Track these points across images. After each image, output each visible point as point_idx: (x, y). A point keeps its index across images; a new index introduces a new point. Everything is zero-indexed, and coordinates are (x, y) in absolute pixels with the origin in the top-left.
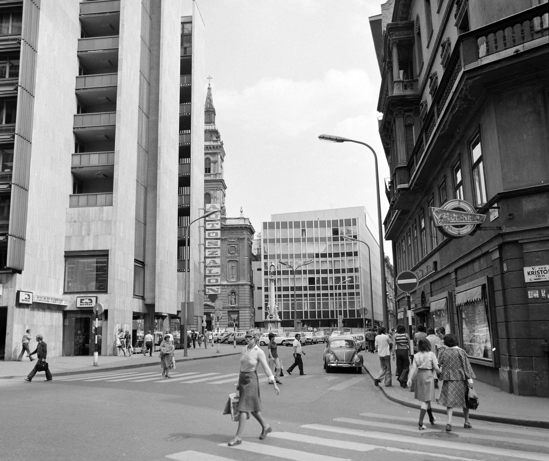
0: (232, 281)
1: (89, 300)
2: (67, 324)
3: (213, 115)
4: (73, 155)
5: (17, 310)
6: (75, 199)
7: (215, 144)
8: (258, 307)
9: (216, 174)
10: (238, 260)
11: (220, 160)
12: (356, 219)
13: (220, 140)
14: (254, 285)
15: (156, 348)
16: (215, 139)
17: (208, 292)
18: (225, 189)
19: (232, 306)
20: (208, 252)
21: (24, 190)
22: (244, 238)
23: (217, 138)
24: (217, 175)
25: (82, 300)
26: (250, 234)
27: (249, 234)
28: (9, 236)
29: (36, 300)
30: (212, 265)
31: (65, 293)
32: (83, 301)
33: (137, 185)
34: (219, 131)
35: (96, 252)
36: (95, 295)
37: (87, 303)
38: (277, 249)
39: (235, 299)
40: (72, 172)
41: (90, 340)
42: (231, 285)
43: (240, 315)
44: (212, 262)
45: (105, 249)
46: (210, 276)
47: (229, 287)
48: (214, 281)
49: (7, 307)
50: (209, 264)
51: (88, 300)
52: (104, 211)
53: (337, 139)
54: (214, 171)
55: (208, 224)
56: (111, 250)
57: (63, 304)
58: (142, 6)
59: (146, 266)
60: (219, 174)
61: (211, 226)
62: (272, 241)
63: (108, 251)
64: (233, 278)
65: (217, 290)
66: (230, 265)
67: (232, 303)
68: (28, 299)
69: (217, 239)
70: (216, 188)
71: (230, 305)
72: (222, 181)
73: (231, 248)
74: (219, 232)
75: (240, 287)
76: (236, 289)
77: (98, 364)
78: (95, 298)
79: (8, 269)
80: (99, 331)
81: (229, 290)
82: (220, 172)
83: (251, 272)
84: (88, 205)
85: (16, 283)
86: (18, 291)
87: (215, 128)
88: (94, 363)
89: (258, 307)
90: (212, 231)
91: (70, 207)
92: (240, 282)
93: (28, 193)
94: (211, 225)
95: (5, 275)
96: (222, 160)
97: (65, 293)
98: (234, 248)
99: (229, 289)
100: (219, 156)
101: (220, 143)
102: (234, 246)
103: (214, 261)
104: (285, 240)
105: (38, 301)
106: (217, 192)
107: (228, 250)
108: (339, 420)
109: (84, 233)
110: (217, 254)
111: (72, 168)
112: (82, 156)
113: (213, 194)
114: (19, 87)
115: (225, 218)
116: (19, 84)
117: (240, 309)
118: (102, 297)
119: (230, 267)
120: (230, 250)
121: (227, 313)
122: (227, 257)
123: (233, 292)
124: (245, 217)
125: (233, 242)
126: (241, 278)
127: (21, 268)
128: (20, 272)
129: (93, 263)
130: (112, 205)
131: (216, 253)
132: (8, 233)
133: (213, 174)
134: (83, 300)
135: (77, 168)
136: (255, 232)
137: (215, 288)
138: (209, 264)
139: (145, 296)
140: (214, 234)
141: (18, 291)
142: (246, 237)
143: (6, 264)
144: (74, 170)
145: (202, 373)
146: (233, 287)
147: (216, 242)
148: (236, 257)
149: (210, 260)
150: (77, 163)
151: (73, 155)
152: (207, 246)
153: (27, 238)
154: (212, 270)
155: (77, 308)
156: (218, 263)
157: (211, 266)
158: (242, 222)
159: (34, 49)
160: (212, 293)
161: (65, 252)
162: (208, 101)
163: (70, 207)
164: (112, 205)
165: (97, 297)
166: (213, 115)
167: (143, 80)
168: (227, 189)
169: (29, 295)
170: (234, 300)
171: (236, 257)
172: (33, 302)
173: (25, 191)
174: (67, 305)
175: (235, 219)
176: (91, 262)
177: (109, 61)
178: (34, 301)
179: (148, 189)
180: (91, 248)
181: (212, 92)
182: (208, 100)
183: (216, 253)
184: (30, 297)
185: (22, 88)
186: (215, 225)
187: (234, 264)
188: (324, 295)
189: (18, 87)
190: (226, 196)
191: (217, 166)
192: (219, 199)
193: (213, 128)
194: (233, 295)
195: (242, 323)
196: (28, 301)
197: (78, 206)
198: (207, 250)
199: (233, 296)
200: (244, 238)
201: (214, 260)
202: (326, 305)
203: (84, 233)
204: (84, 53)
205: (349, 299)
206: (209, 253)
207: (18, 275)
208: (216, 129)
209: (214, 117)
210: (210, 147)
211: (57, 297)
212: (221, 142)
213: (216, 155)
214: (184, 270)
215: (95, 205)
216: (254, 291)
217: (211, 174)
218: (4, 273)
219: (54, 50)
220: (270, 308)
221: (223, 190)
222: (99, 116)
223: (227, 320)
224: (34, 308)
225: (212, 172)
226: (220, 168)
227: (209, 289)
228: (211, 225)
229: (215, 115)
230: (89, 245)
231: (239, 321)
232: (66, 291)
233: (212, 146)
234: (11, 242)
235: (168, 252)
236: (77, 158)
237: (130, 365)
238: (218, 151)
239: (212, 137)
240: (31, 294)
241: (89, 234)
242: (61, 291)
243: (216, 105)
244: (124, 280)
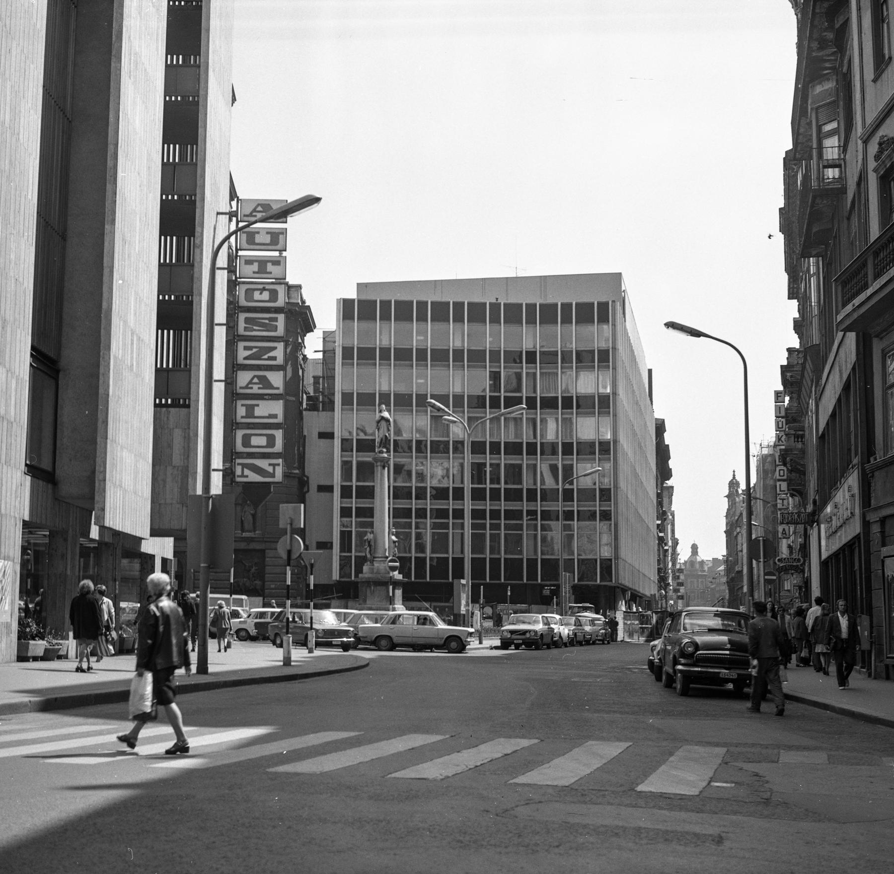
8: (318, 543)
12: (607, 303)
14: (308, 478)
17: (243, 476)
20: (246, 348)
30: (255, 389)
35: (203, 129)
38: (380, 376)
39: (254, 516)
44: (256, 380)
46: (249, 426)
59: (61, 375)
61: (256, 270)
62: (367, 354)
65: (270, 469)
83: (302, 441)
89: (318, 543)
104: (403, 355)
131: (272, 354)
136: (315, 327)
137: (263, 464)
138: (247, 387)
139: (57, 471)
147: (270, 319)
152: (241, 331)
154: (258, 405)
156: (275, 386)
160: (254, 477)
170: (250, 518)
183: (272, 354)
188: (509, 514)
195: (273, 586)
198: (241, 345)
199: (246, 508)
201: (265, 377)
202: (515, 542)
205: (507, 527)
206: (248, 353)
216: (307, 495)
227: (244, 466)
231: (263, 581)
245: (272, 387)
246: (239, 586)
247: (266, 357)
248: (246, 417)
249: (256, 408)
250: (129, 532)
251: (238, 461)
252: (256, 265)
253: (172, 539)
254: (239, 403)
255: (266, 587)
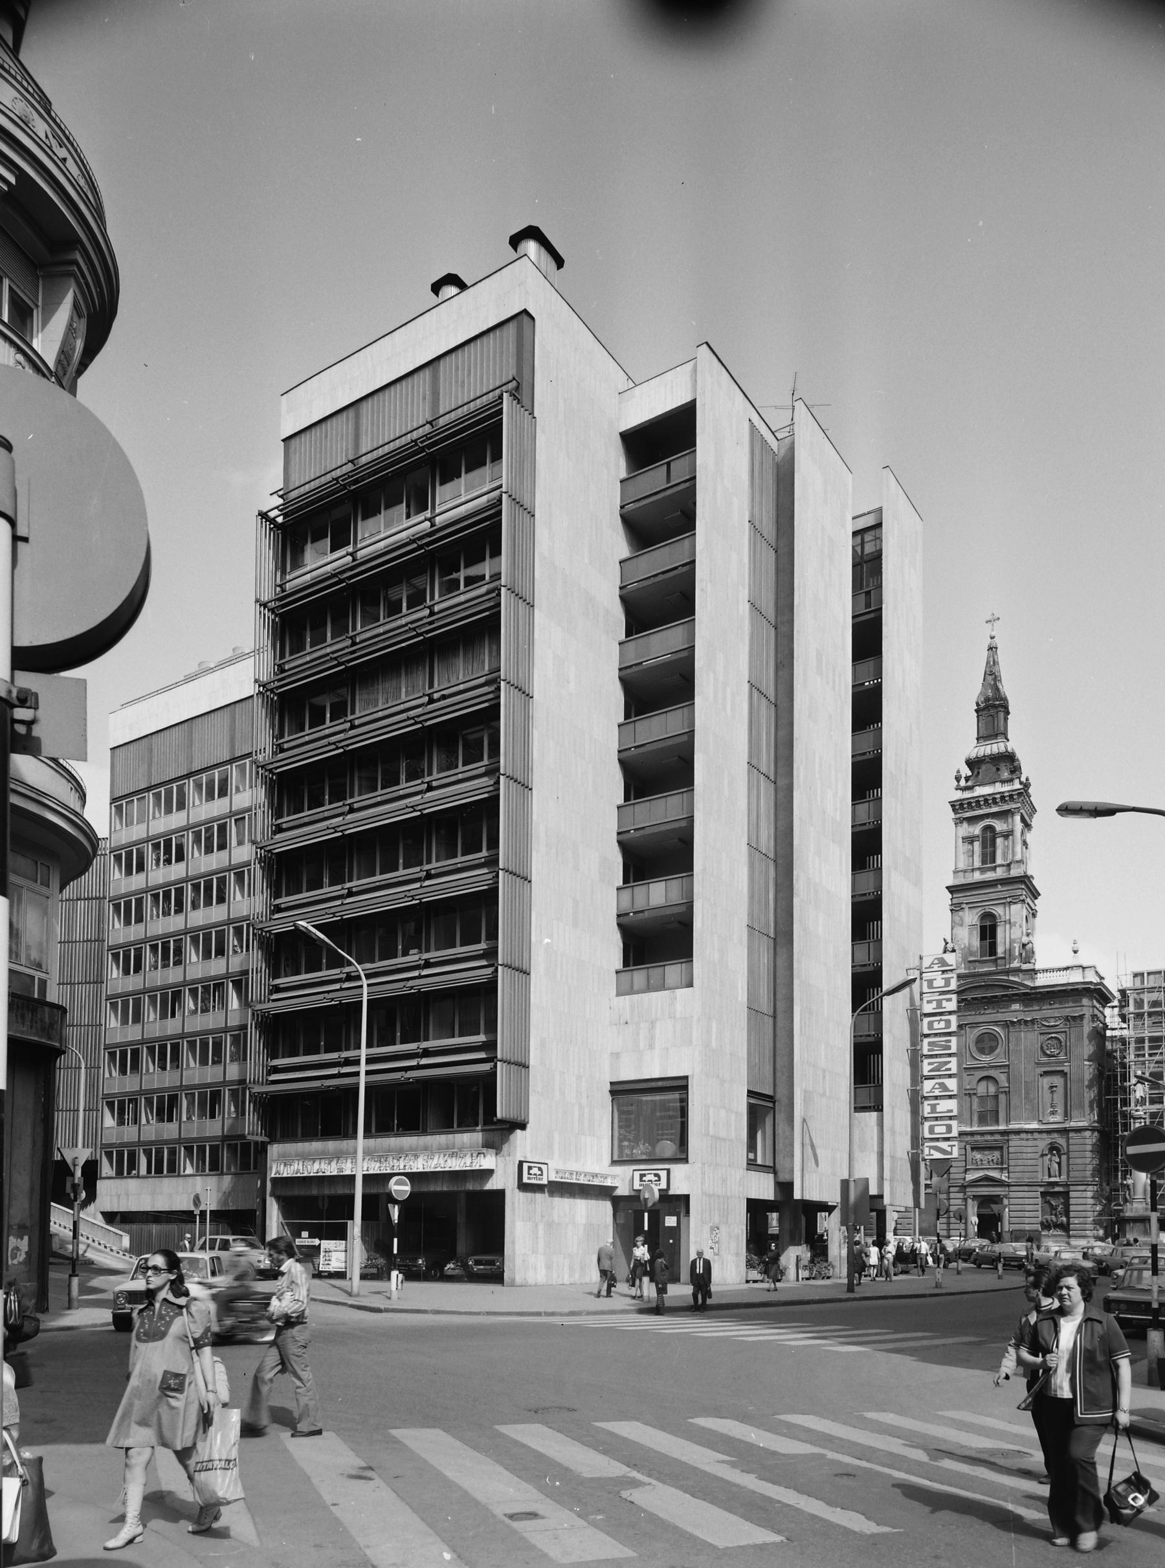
0: (1052, 1120)
1: (656, 1175)
2: (621, 1221)
3: (1002, 715)
4: (618, 889)
5: (522, 1196)
6: (626, 976)
7: (1006, 788)
9: (1009, 865)
10: (1066, 1069)
11: (1019, 826)
13: (1019, 778)
15: (749, 1274)
16: (1006, 775)
18: (1036, 898)
19: (1052, 1179)
21: (521, 974)
22: (1082, 1017)
23: (1012, 772)
24: (1012, 866)
25: (642, 1176)
26: (1100, 1003)
27: (1098, 1005)
28: (498, 1063)
29: (553, 1178)
30: (937, 1093)
31: (614, 1162)
32: (644, 1179)
33: (750, 936)
34: (1019, 755)
36: (667, 1166)
37: (651, 1181)
39: (1059, 1164)
40: (619, 925)
41: (976, 1230)
42: (1049, 1132)
43: (1072, 1201)
44: (937, 1086)
45: (681, 1075)
47: (1044, 1136)
48: (943, 1130)
49: (504, 1190)
50: (931, 1092)
51: (652, 1175)
52: (678, 997)
53: (1083, 808)
54: (1005, 857)
55: (929, 1002)
56: (693, 1076)
57: (609, 1184)
58: (750, 529)
60: (1017, 862)
61: (935, 1007)
63: (686, 1078)
64: (1053, 1113)
65: (949, 1149)
66: (1046, 1081)
67: (1052, 1174)
68: (539, 1175)
69: (950, 1034)
70: (1008, 900)
71: (1046, 1179)
72: (1025, 880)
73: (1049, 1042)
74: (953, 1019)
75: (1071, 1135)
76: (1062, 1141)
77: (943, 1286)
78: (666, 1171)
79: (501, 1121)
80: (675, 1232)
81: (1043, 1143)
82: (1018, 857)
84: (649, 989)
85: (516, 1147)
86: (520, 1161)
87: (1006, 747)
88: (937, 1283)
90: (938, 1018)
91: (619, 994)
92: (1073, 1124)
93: (530, 979)
94: (935, 1003)
95: (497, 1134)
96: (1027, 825)
97: (614, 1162)
98: (1055, 1042)
99: (1044, 1139)
100: (1018, 818)
101: (1021, 783)
102: (1055, 1038)
103: (943, 1087)
105: (558, 1180)
106: (1013, 907)
107: (1042, 1048)
108: (631, 1430)
109: (642, 1044)
110: (950, 1069)
111: (619, 916)
112: (635, 892)
113: (1002, 913)
114: (501, 777)
115: (1033, 970)
116: (502, 771)
117: (1072, 1188)
118: (677, 1170)
119: (1046, 1086)
120: (1045, 1047)
121: (1039, 1196)
122: (1038, 1064)
123: (1054, 1148)
124: (1084, 965)
125: (1052, 1026)
126: (1075, 1113)
127: (523, 1118)
128: (523, 1126)
129: (673, 1101)
130: (691, 986)
131: (947, 1067)
132: (496, 1057)
133: (1003, 866)
134: (644, 1175)
135: (631, 914)
137: (944, 1145)
138: (931, 1092)
139: (777, 1166)
140: (942, 1024)
141: (520, 1161)
142: (1087, 1012)
143: (496, 1115)
144: (624, 920)
145: (857, 1329)
146: (1055, 1135)
148: (1061, 1063)
149: (932, 1082)
150: (626, 905)
151: (618, 889)
153: (533, 1062)
155: (634, 1190)
157: (936, 1098)
158: (1075, 977)
159: (527, 693)
160: (937, 1155)
161: (611, 1083)
162: (990, 678)
163: (619, 994)
164: (691, 986)
165: (668, 1171)
166: (1002, 715)
167: (759, 699)
168: (1039, 897)
169: (540, 1169)
171: (1061, 1063)
172: (549, 1182)
173: (524, 976)
174: (617, 1185)
175: (1059, 970)
176: (669, 1101)
177: (680, 675)
178: (550, 1179)
179: (778, 940)
180: (656, 1075)
181: (1001, 656)
182: (990, 678)
183: (947, 1067)
184: (542, 1172)
185: (507, 777)
186: (944, 1002)
187: (1058, 1081)
189: (499, 778)
190: (1038, 914)
191: (1010, 842)
192: (1017, 925)
193: (1002, 749)
194: (1054, 1155)
195: (1076, 1222)
196: (540, 1179)
197: (631, 991)
199: (1053, 1158)
200: (1082, 1017)
203: (642, 1044)
204: (635, 669)
206: (931, 1067)
207: (518, 1132)
208: (1009, 750)
209: (1006, 719)
210: (994, 799)
211: (597, 1171)
212: (1023, 779)
213: (1010, 815)
214: (880, 1107)
215: (662, 987)
217: (996, 867)
218: (497, 1130)
219: (568, 682)
220: (1131, 1187)
221: (1028, 900)
222: (664, 799)
223: (1040, 1212)
224: (553, 1192)
225: (999, 861)
226: (1019, 847)
227: (931, 1147)
228: (934, 1004)
229: (1008, 713)
230: (653, 1069)
231: (1068, 1217)
232: (616, 1158)
233: (998, 796)
234: (502, 1072)
235: (824, 1071)
236: (626, 894)
237: (883, 1295)
238: (1014, 806)
239: (999, 773)
240: (544, 1167)
241: (651, 1047)
242: (607, 1160)
243: (1008, 688)
244: (723, 1134)
245: (948, 1090)
246: (1047, 1221)
247: (944, 1069)
248: (932, 1113)
249: (938, 1106)
250: (818, 1200)
251: (926, 1144)
252: (935, 1003)
253: (675, 1225)
254: (926, 1103)
255: (1071, 1222)
